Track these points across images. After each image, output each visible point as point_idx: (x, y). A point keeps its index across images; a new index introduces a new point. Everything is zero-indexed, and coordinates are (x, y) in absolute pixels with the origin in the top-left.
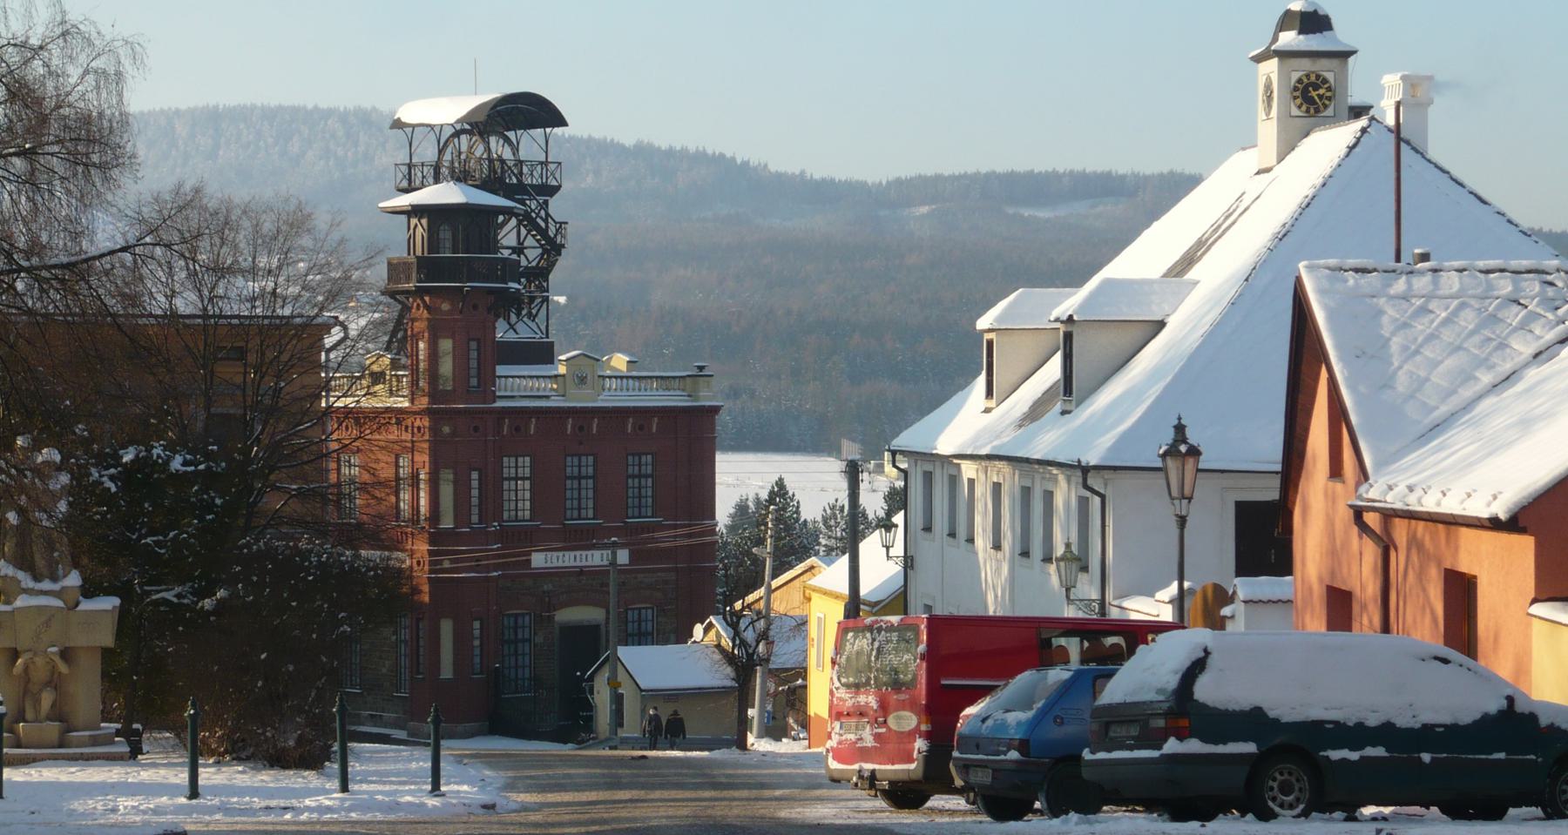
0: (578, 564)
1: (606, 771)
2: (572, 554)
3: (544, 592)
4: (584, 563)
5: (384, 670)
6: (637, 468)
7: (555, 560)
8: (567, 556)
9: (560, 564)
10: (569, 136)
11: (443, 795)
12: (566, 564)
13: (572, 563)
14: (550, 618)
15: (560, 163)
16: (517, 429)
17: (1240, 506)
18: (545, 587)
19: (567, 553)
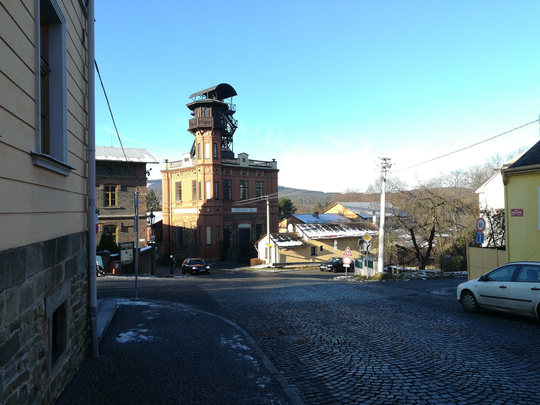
0: (244, 211)
1: (50, 391)
2: (242, 209)
3: (235, 219)
4: (245, 211)
5: (189, 242)
6: (258, 186)
7: (238, 210)
8: (238, 210)
9: (239, 211)
10: (478, 195)
11: (318, 218)
12: (241, 211)
13: (242, 211)
14: (237, 227)
15: (235, 105)
16: (259, 175)
17: (236, 95)
18: (235, 218)
19: (241, 209)
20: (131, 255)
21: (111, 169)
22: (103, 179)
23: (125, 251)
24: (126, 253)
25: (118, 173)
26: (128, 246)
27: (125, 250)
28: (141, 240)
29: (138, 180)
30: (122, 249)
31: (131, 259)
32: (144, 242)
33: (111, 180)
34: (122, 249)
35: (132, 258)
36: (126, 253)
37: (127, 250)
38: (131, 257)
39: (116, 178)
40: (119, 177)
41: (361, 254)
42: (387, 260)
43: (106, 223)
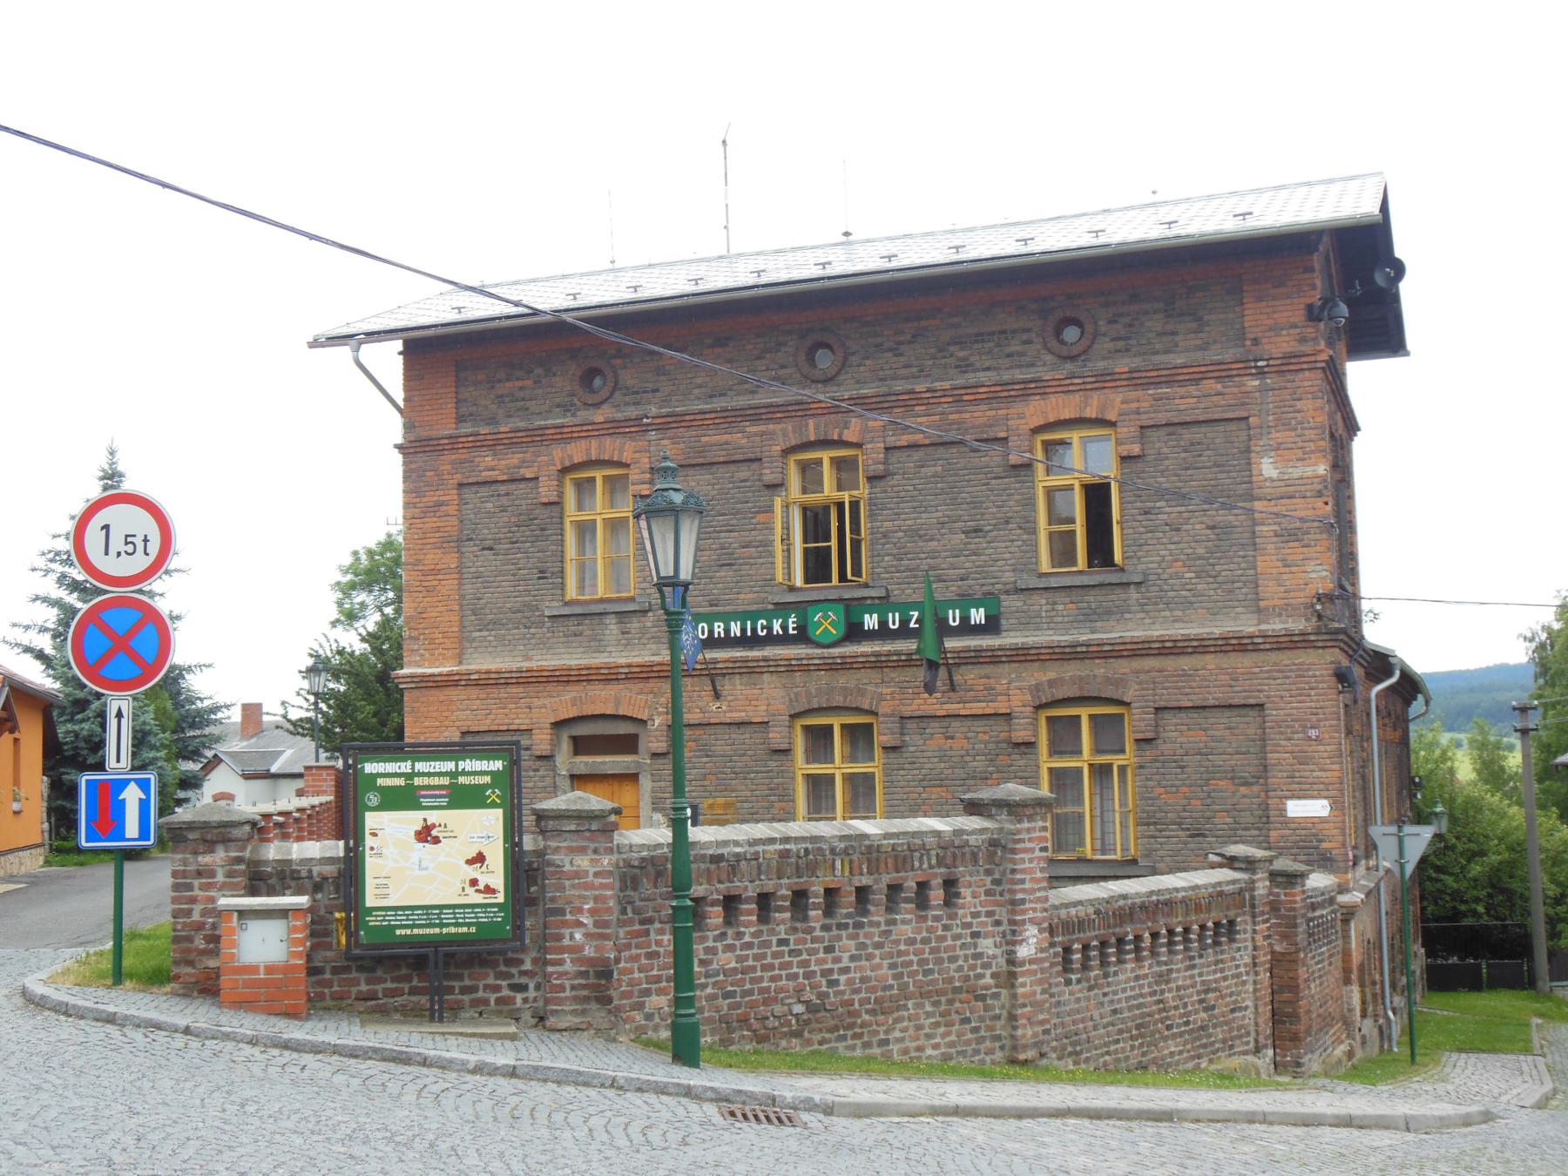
20: (479, 859)
21: (1077, 322)
22: (1025, 395)
23: (412, 820)
24: (426, 835)
25: (1121, 344)
26: (453, 775)
27: (420, 815)
28: (1297, 809)
29: (1261, 373)
30: (373, 799)
31: (479, 899)
32: (1322, 820)
33: (1077, 398)
34: (373, 799)
35: (489, 890)
36: (426, 835)
37: (433, 817)
38: (483, 881)
39: (1104, 380)
40: (1122, 365)
41: (207, 731)
42: (242, 892)
43: (1051, 683)
